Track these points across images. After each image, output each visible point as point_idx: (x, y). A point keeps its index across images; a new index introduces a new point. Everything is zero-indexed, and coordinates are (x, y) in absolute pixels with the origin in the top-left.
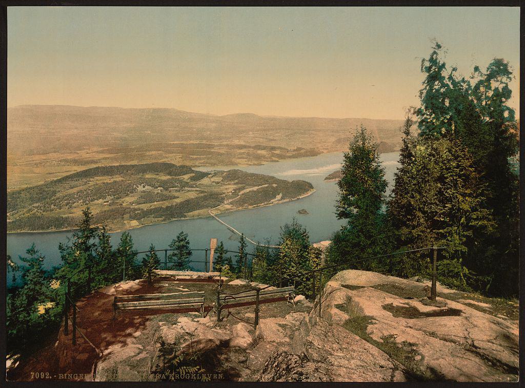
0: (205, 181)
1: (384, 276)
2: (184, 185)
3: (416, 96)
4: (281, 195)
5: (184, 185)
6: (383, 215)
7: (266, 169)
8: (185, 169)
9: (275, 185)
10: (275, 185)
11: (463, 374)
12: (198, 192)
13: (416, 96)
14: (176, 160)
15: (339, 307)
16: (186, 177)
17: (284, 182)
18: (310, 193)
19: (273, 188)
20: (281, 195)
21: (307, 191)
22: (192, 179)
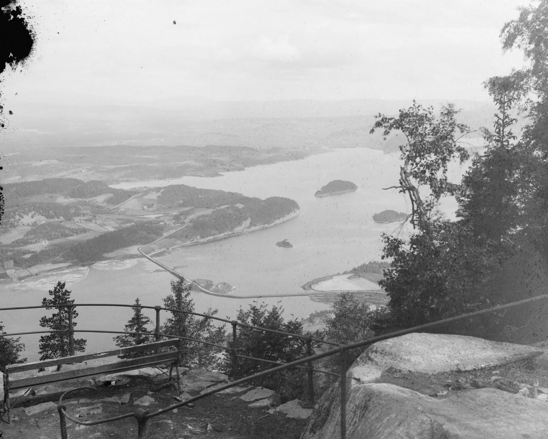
0: (131, 204)
1: (92, 179)
2: (97, 211)
3: (285, 244)
4: (248, 221)
5: (97, 211)
6: (447, 226)
7: (228, 182)
8: (97, 188)
9: (240, 206)
10: (240, 206)
11: (424, 370)
12: (119, 222)
13: (285, 244)
14: (84, 174)
15: (339, 377)
16: (100, 199)
17: (255, 200)
18: (292, 215)
19: (237, 210)
20: (248, 221)
21: (289, 212)
22: (110, 201)
